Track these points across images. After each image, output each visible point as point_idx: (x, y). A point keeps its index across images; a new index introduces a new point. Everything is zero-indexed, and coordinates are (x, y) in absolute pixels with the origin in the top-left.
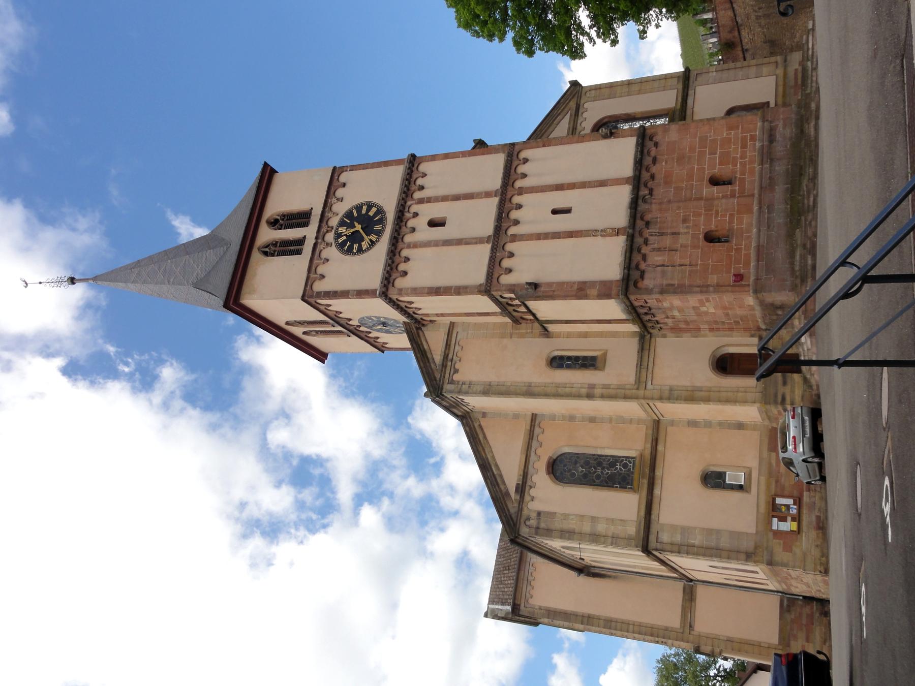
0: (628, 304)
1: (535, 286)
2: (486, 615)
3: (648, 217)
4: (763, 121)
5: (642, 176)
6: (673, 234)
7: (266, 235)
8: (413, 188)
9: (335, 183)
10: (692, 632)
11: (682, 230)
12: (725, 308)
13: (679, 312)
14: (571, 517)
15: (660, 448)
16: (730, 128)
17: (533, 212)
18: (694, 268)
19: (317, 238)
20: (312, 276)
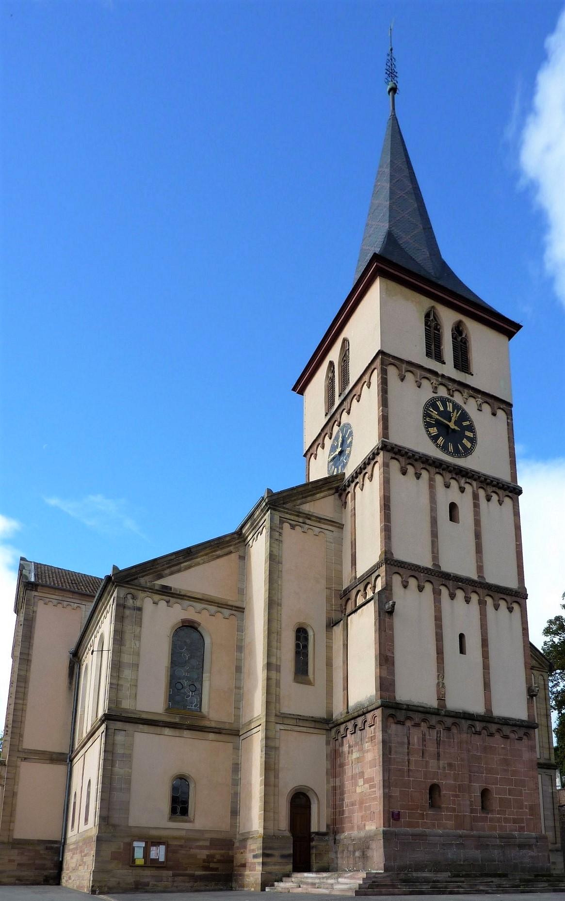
0: (370, 708)
1: (391, 612)
2: (22, 559)
3: (454, 730)
4: (536, 838)
5: (493, 725)
6: (438, 754)
7: (448, 318)
8: (490, 489)
9: (496, 404)
10: (19, 760)
11: (441, 762)
13: (358, 758)
14: (137, 643)
15: (212, 736)
17: (462, 614)
18: (406, 774)
19: (443, 376)
20: (404, 366)
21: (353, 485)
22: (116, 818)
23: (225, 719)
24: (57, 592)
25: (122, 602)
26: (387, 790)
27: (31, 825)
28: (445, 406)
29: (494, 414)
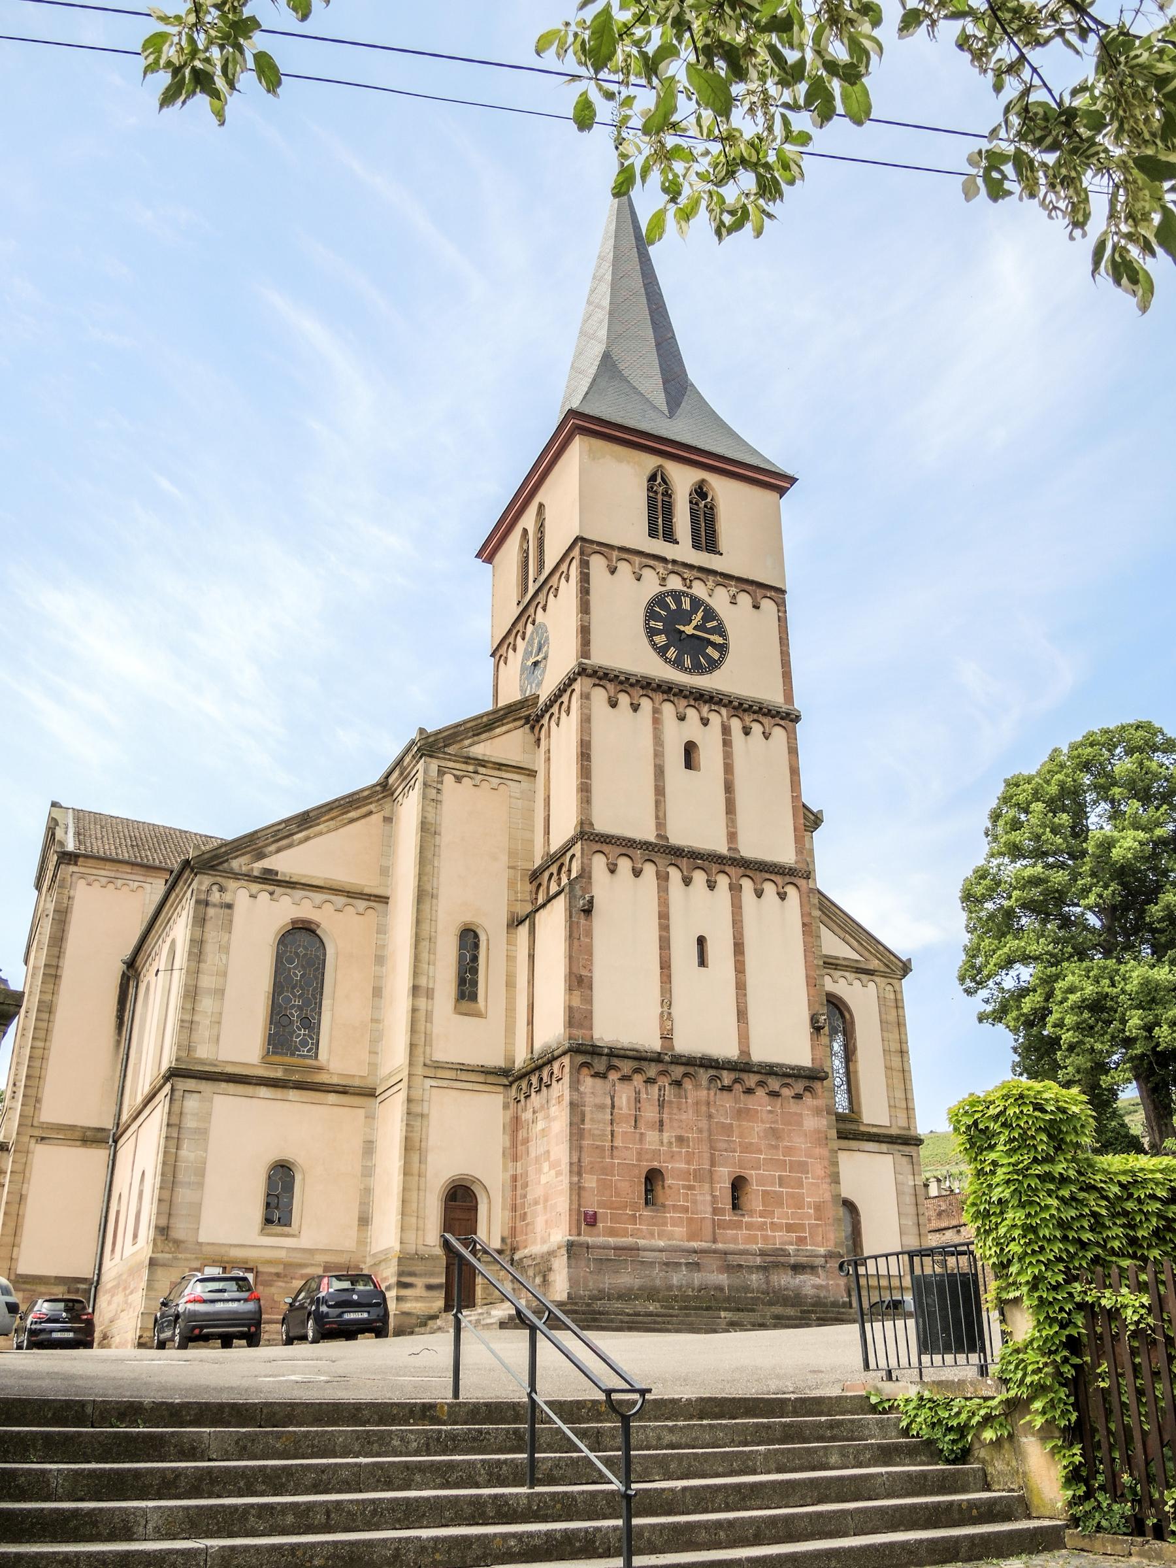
0: (556, 1053)
1: (588, 911)
3: (688, 1084)
4: (825, 1256)
5: (751, 1075)
6: (661, 1123)
8: (748, 718)
10: (33, 1141)
11: (666, 1135)
12: (546, 1200)
14: (224, 957)
15: (332, 1098)
16: (818, 1207)
18: (607, 1153)
19: (674, 562)
20: (615, 553)
21: (547, 716)
22: (180, 1231)
23: (353, 1071)
24: (108, 866)
25: (203, 897)
26: (576, 1179)
27: (51, 1247)
28: (678, 602)
29: (756, 607)
